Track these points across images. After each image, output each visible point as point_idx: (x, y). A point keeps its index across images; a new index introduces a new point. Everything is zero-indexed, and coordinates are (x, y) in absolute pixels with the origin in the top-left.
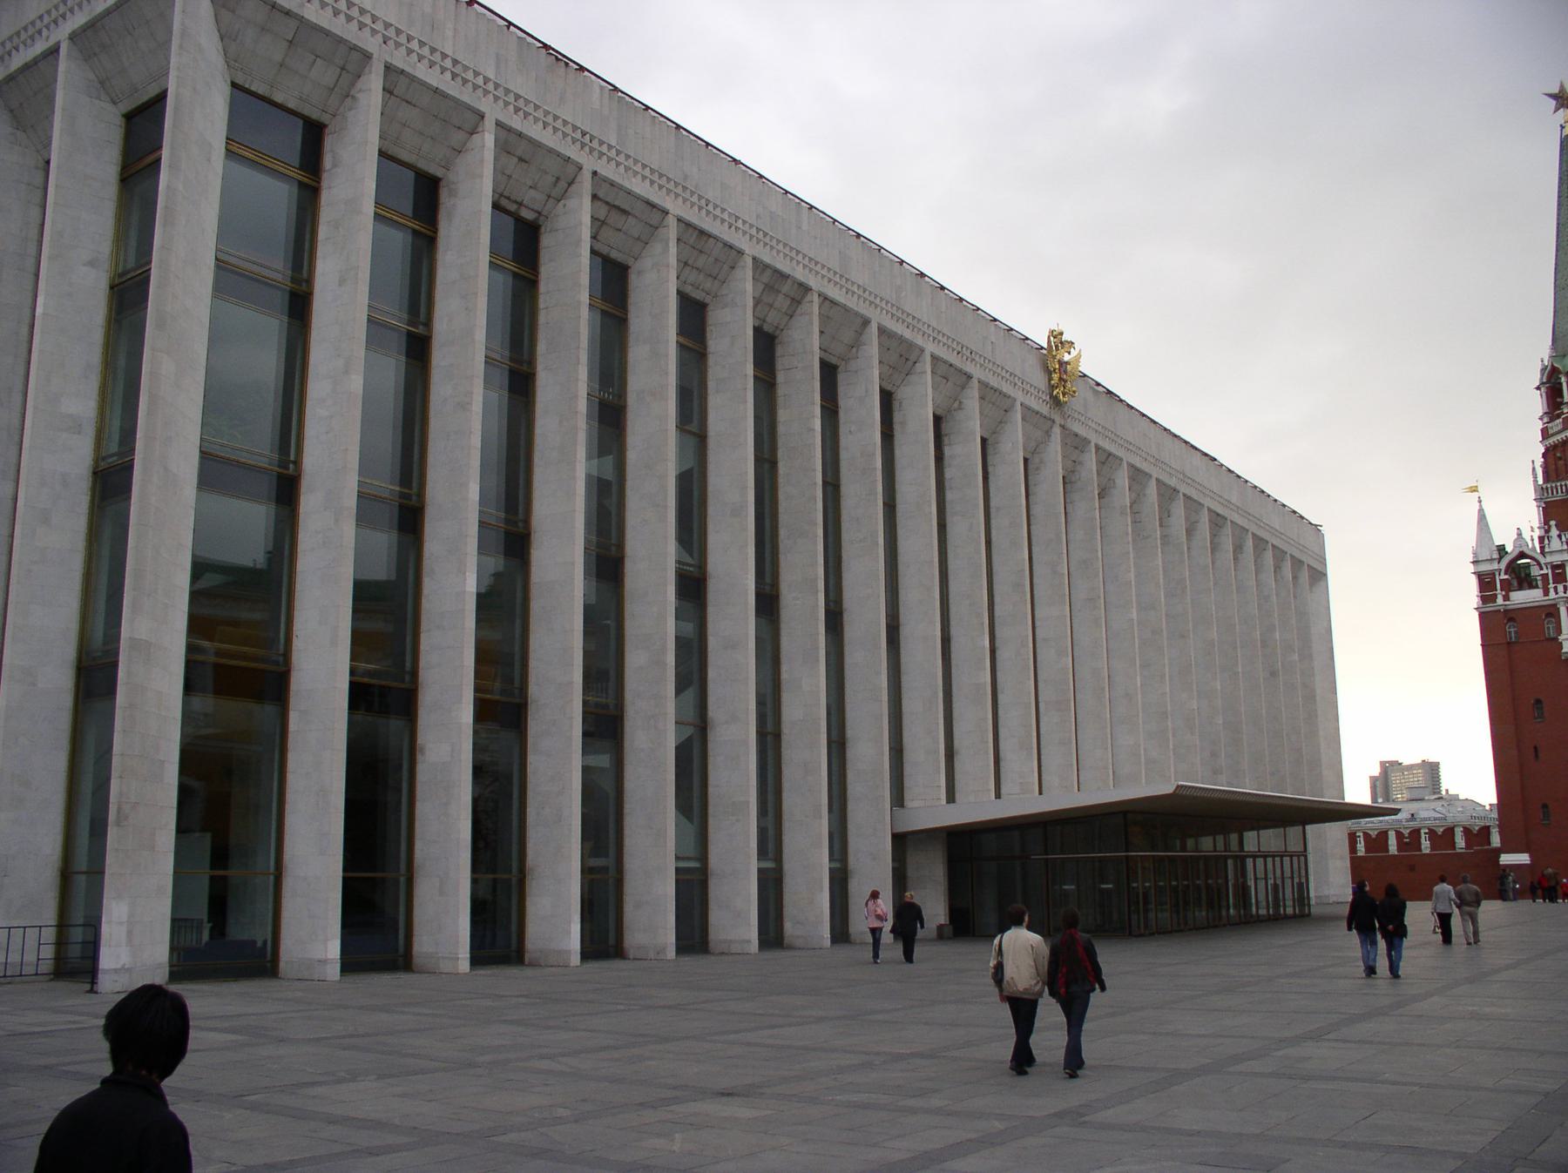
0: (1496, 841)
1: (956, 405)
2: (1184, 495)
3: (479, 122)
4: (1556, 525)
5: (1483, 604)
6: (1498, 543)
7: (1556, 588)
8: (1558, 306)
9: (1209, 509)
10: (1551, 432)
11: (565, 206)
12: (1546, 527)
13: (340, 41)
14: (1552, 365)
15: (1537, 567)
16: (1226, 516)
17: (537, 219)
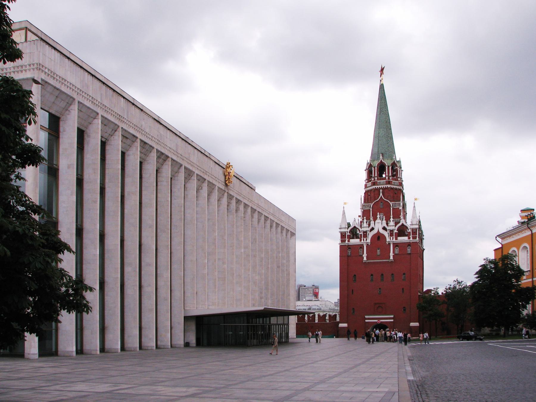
1: (200, 188)
2: (258, 211)
3: (97, 116)
4: (366, 218)
5: (341, 242)
6: (348, 222)
9: (264, 215)
10: (367, 186)
11: (114, 138)
12: (363, 218)
13: (68, 96)
14: (370, 163)
15: (359, 232)
16: (269, 217)
17: (105, 141)
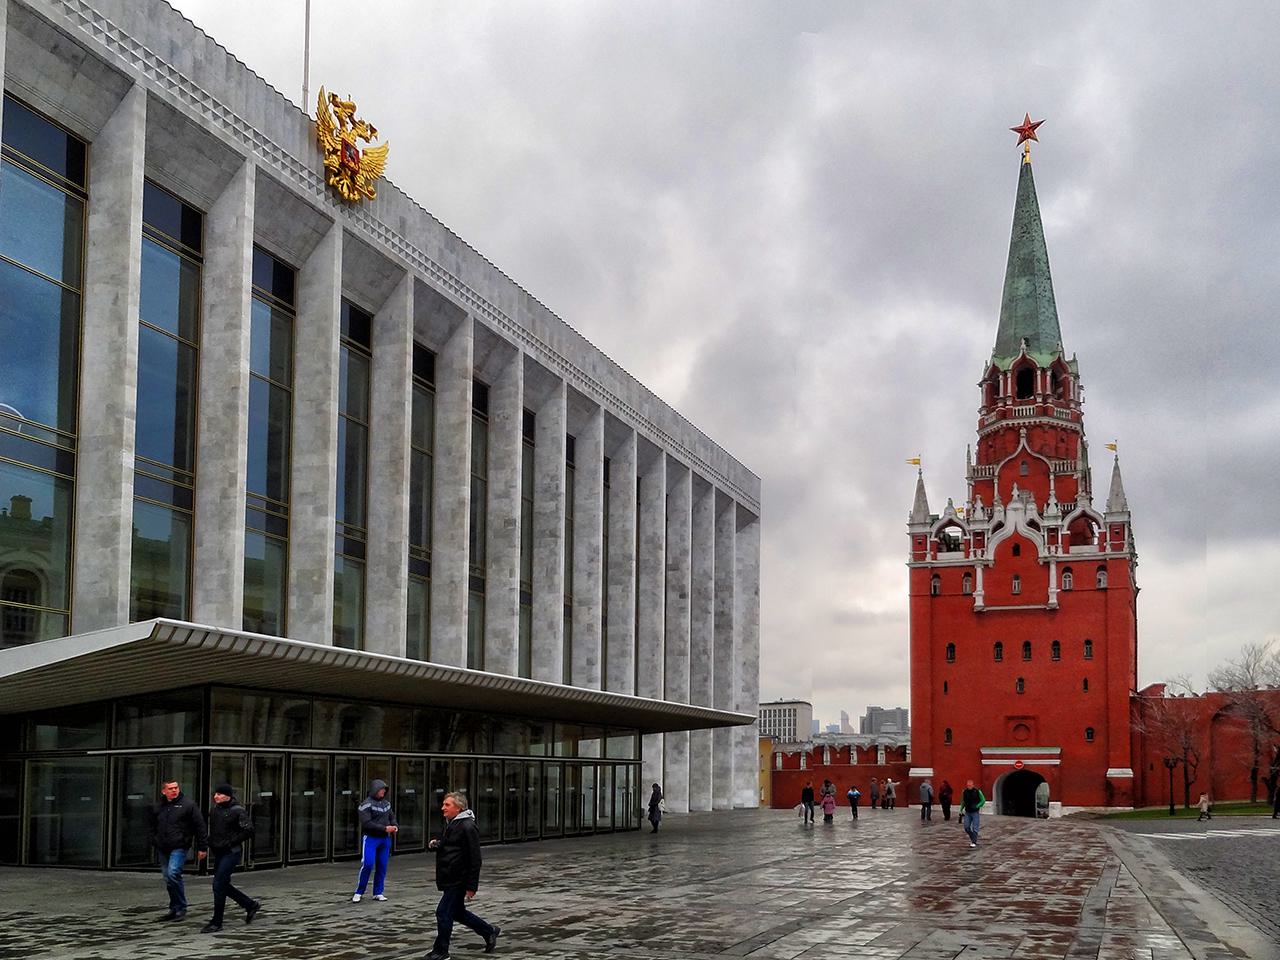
0: (909, 759)
7: (975, 552)
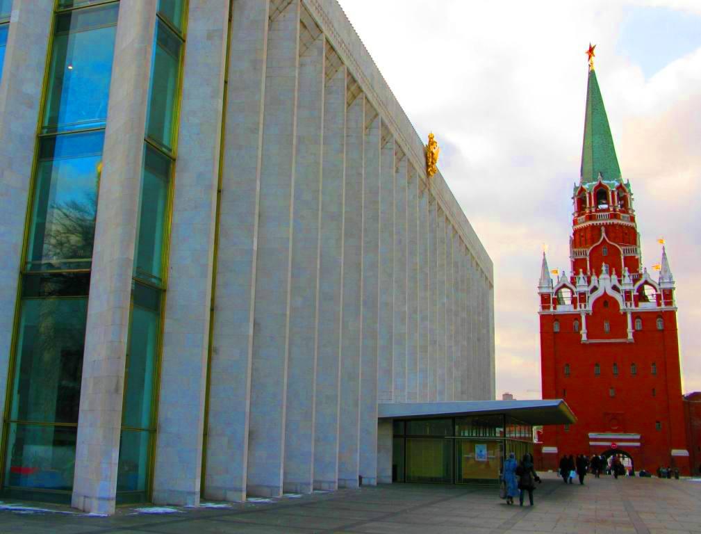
8: (586, 160)
